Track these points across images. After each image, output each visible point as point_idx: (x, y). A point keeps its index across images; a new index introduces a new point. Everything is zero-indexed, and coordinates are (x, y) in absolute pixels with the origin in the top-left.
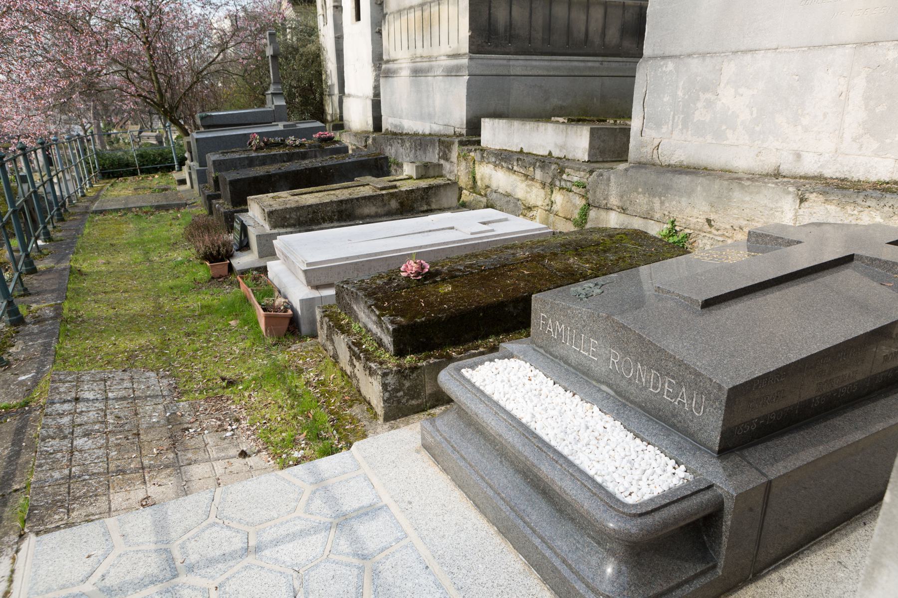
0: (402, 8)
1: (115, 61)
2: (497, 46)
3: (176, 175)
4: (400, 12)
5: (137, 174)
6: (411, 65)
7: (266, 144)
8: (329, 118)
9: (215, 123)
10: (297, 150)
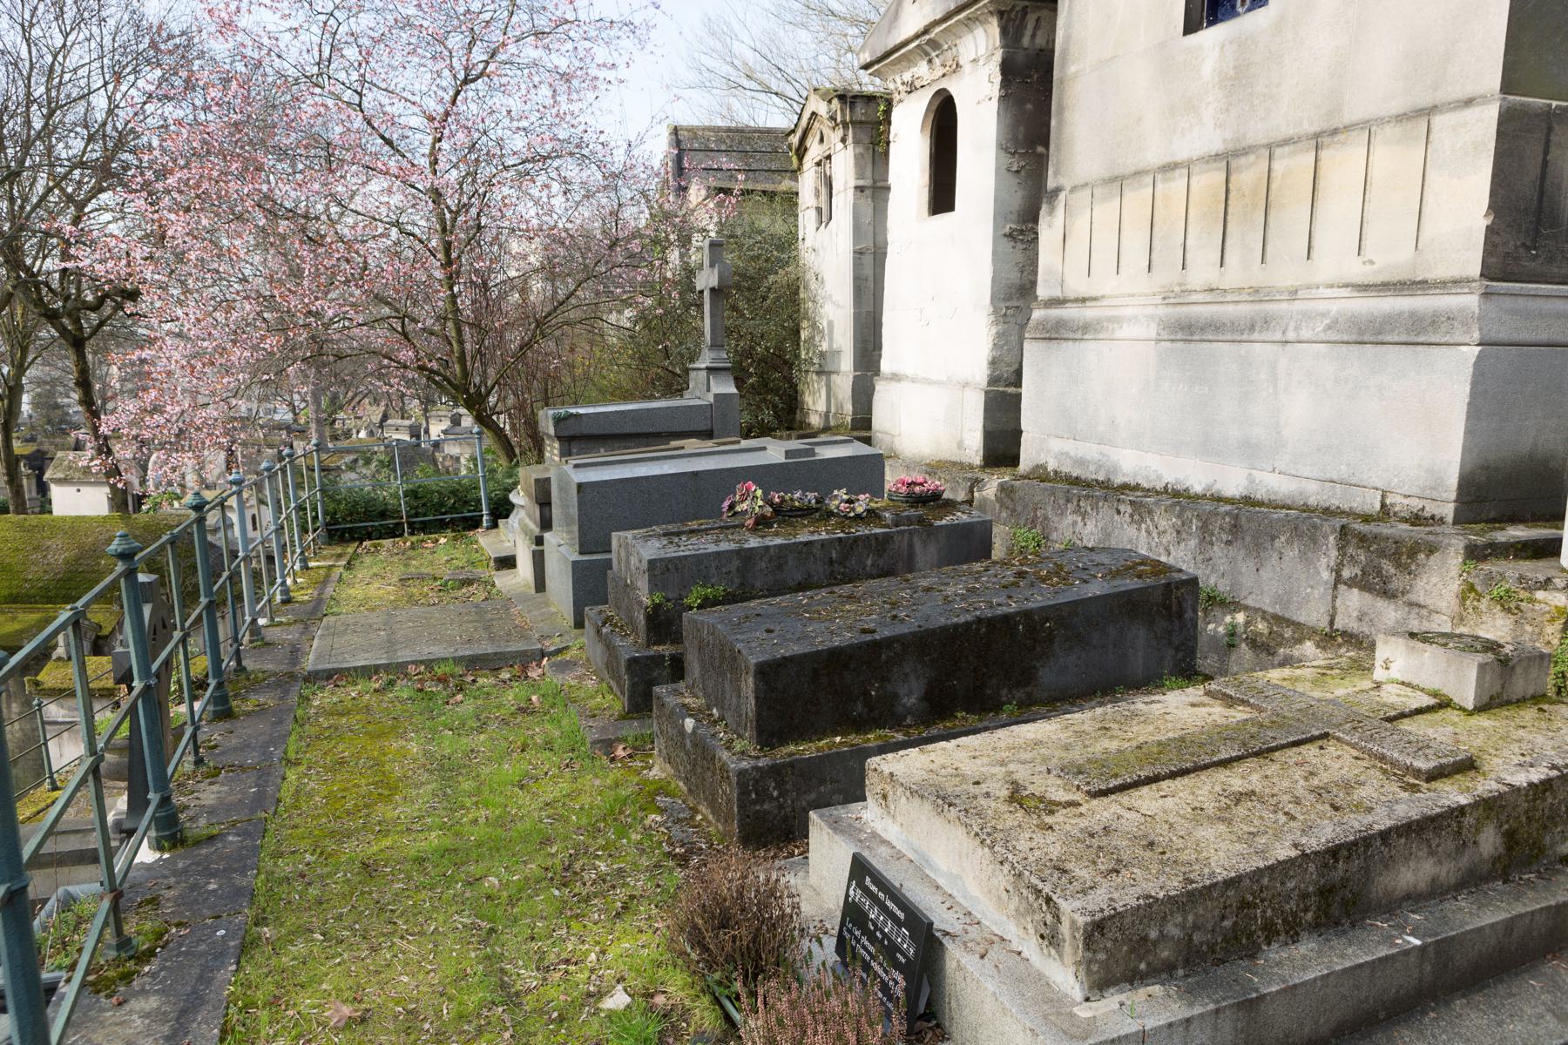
0: (1128, 164)
1: (380, 300)
2: (1551, 260)
3: (489, 542)
4: (1118, 182)
5: (401, 535)
6: (1162, 311)
7: (778, 510)
8: (815, 420)
9: (586, 431)
10: (862, 531)
